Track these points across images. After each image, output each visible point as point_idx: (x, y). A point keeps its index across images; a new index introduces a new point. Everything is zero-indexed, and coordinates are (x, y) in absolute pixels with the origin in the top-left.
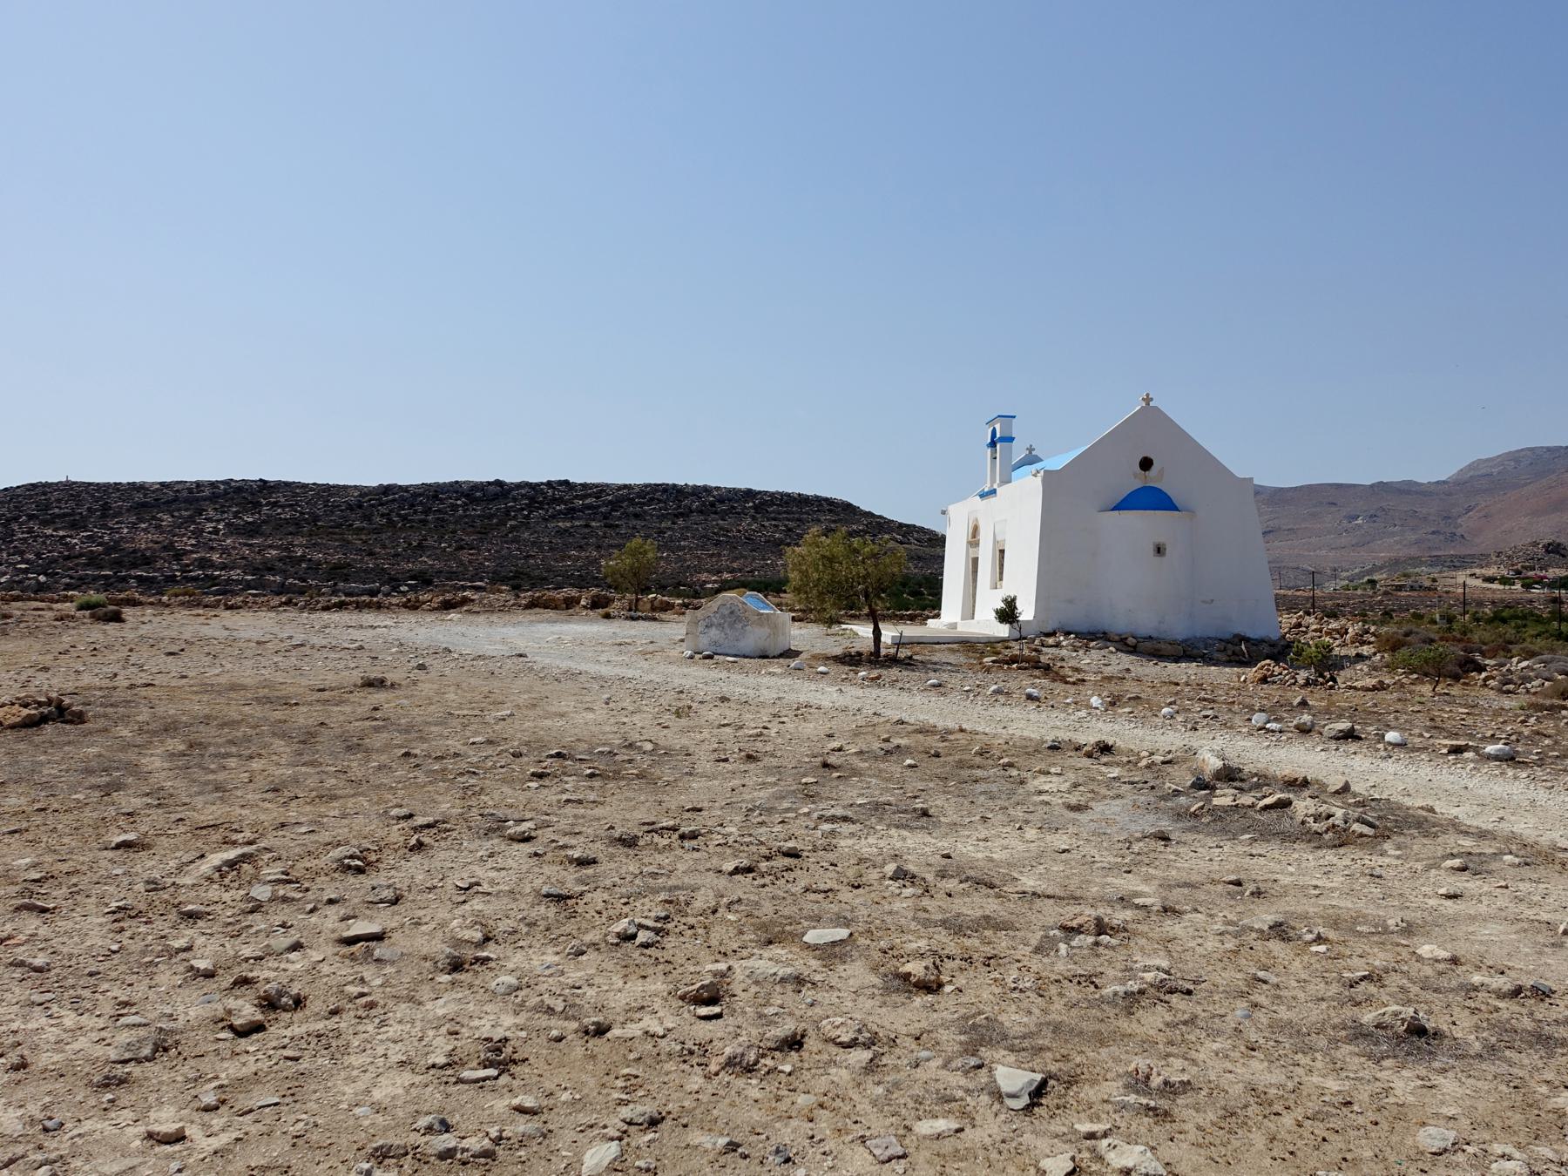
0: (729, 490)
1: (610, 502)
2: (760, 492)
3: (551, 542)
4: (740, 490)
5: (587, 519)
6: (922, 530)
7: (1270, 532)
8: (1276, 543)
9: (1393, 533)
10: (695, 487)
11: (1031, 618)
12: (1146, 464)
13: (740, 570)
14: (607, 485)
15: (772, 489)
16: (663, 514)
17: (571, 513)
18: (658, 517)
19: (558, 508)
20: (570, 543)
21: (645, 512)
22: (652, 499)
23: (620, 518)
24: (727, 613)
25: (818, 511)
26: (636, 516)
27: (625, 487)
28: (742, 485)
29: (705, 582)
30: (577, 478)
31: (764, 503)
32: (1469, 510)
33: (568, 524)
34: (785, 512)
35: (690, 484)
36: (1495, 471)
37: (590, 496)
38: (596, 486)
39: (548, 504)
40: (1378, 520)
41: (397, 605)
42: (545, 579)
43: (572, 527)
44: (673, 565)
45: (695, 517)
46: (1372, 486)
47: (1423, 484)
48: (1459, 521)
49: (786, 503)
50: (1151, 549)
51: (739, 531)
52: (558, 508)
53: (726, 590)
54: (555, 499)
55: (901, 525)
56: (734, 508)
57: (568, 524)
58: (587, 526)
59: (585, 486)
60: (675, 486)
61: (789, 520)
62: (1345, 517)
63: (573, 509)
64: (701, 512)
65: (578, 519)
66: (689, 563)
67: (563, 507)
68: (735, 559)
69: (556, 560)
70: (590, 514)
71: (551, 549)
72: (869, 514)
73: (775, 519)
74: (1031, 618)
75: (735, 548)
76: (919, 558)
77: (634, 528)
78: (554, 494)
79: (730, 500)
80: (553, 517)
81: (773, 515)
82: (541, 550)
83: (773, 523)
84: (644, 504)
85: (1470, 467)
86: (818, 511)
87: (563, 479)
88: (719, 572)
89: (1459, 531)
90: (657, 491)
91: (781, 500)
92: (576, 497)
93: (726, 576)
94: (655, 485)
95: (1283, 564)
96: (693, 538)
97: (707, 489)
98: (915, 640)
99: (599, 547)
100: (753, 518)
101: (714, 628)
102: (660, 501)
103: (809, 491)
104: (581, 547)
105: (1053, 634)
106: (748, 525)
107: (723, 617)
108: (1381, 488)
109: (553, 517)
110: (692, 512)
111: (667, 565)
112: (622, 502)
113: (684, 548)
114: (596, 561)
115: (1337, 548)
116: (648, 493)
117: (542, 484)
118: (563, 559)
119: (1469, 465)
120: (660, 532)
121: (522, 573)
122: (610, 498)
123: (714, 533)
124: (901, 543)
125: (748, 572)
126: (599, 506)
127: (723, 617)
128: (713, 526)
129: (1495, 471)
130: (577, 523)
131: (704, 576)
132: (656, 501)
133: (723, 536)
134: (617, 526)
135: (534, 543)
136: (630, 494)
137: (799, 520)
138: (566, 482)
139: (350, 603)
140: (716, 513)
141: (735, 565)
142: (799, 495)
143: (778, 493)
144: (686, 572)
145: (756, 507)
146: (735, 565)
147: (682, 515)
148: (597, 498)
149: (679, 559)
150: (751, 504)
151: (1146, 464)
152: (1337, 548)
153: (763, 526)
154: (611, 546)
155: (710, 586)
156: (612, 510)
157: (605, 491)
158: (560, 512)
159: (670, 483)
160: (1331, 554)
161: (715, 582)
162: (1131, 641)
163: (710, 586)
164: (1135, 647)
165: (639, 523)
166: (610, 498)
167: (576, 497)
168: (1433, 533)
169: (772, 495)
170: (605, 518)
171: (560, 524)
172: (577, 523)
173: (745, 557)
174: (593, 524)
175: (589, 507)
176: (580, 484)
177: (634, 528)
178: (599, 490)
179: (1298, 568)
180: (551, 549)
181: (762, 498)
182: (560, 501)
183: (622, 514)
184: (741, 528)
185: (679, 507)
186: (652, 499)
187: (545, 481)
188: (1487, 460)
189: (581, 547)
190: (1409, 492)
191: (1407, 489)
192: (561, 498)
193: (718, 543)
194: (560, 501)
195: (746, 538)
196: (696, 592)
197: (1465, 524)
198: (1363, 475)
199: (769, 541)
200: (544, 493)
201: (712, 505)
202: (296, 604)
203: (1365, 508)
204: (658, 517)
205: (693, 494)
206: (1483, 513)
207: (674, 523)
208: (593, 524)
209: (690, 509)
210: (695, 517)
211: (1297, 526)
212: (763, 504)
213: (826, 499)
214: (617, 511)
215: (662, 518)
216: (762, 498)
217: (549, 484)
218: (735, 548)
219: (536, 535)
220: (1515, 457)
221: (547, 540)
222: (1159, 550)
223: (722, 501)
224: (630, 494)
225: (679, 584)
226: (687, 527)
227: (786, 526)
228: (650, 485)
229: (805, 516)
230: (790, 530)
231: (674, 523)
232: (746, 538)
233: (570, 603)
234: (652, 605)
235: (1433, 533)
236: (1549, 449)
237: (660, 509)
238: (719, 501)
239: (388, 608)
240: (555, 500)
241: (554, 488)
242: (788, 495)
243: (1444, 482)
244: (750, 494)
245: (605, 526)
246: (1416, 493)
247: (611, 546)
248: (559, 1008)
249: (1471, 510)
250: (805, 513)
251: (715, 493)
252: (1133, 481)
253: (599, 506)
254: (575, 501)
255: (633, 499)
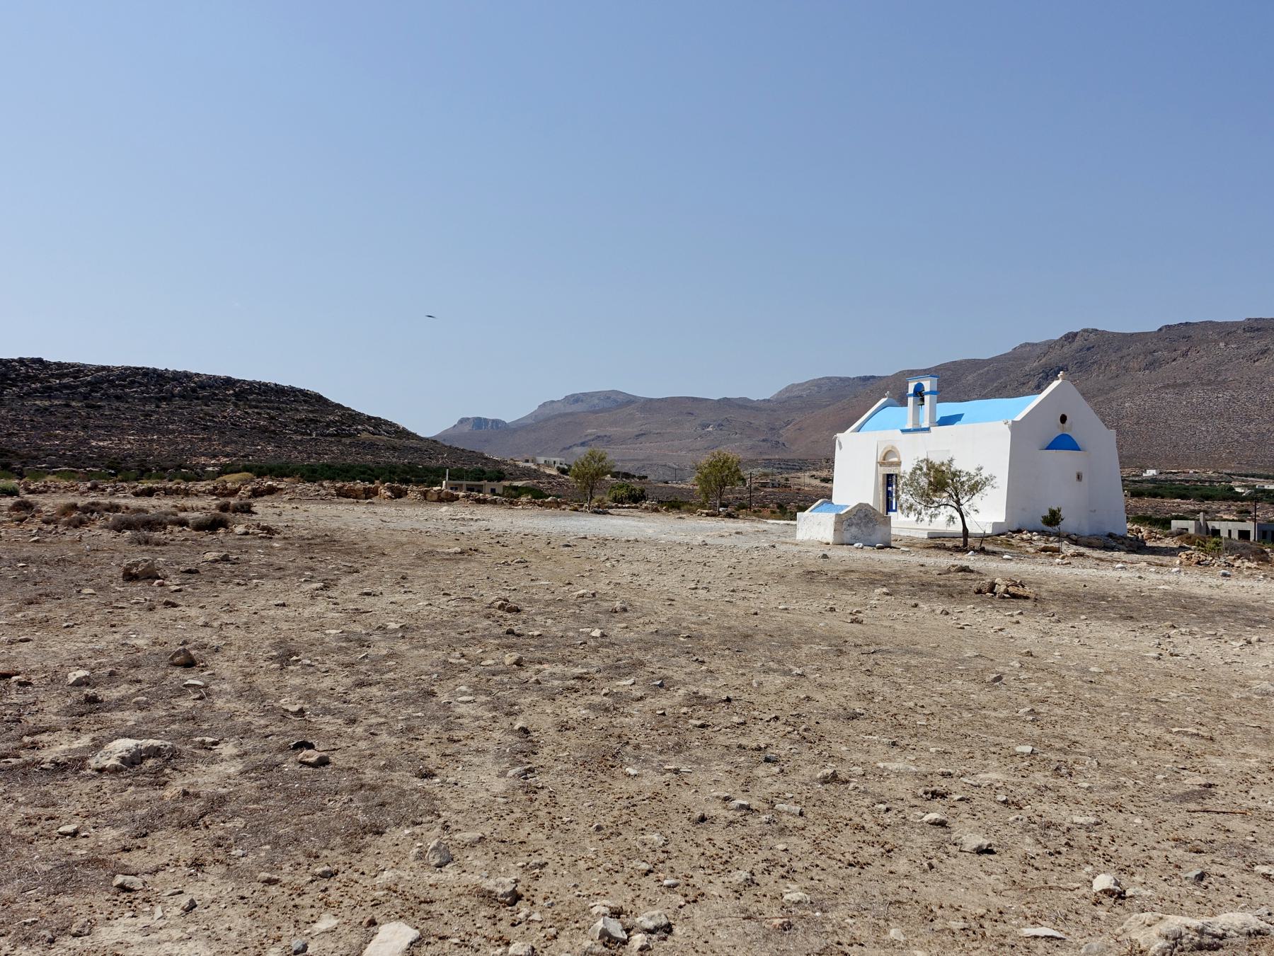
0: (209, 377)
1: (89, 382)
2: (239, 381)
3: (32, 421)
4: (219, 377)
5: (66, 399)
6: (392, 425)
7: (643, 434)
8: (648, 444)
9: (735, 439)
10: (175, 373)
11: (1003, 521)
12: (1063, 419)
13: (235, 455)
14: (84, 366)
15: (249, 379)
16: (145, 397)
17: (48, 392)
18: (140, 400)
19: (33, 386)
20: (53, 422)
21: (126, 394)
22: (133, 382)
23: (101, 399)
24: (862, 515)
25: (294, 401)
26: (118, 398)
27: (104, 368)
28: (222, 372)
29: (205, 466)
30: (51, 357)
31: (243, 391)
32: (788, 423)
33: (47, 403)
34: (264, 401)
35: (171, 369)
36: (804, 394)
37: (67, 375)
38: (73, 366)
39: (22, 381)
40: (724, 428)
41: (204, 492)
42: (36, 458)
43: (51, 406)
44: (167, 447)
45: (177, 402)
46: (719, 401)
47: (754, 401)
48: (781, 432)
49: (264, 392)
50: (1076, 476)
51: (225, 417)
52: (33, 386)
53: (227, 474)
54: (30, 377)
55: (370, 418)
56: (216, 395)
57: (47, 403)
58: (68, 406)
59: (60, 365)
60: (155, 370)
61: (269, 409)
62: (700, 425)
63: (50, 388)
64: (183, 397)
65: (56, 398)
66: (182, 446)
67: (39, 385)
68: (226, 444)
69: (41, 439)
70: (68, 394)
71: (33, 427)
72: (339, 406)
73: (256, 407)
74: (1003, 521)
75: (223, 433)
76: (394, 448)
77: (117, 409)
78: (27, 372)
79: (211, 387)
80: (28, 394)
81: (254, 403)
82: (21, 425)
83: (256, 410)
84: (124, 386)
85: (787, 389)
86: (294, 401)
87: (36, 356)
88: (214, 456)
89: (781, 440)
90: (138, 374)
91: (260, 389)
92: (52, 376)
93: (224, 460)
94: (134, 368)
95: (654, 462)
96: (181, 421)
97: (187, 376)
98: (936, 536)
99: (85, 427)
100: (236, 405)
101: (854, 527)
102: (141, 384)
103: (285, 382)
104: (65, 426)
105: (1019, 531)
106: (232, 411)
107: (860, 518)
108: (726, 402)
109: (28, 394)
110: (173, 396)
111: (160, 447)
112: (102, 383)
113: (173, 432)
114: (84, 442)
115: (693, 450)
116: (129, 376)
117: (14, 360)
118: (49, 437)
119: (786, 388)
120: (147, 415)
121: (9, 451)
122: (89, 379)
123: (200, 418)
124: (374, 434)
125: (242, 456)
126: (78, 387)
127: (860, 518)
128: (198, 411)
129: (804, 394)
130: (56, 402)
131: (202, 460)
132: (137, 385)
133: (210, 421)
134: (100, 407)
135: (13, 421)
136: (109, 376)
137: (278, 408)
138: (40, 361)
139: (159, 489)
140: (198, 398)
141: (228, 449)
142: (276, 385)
143: (255, 382)
144: (181, 455)
145: (236, 395)
146: (228, 449)
147: (164, 399)
148: (75, 378)
149: (171, 442)
150: (231, 392)
151: (1063, 419)
152: (693, 450)
153: (246, 413)
154: (98, 427)
155: (211, 469)
156: (92, 391)
157: (82, 371)
158: (36, 390)
159: (151, 367)
160: (690, 455)
161: (214, 465)
162: (1074, 537)
163: (211, 469)
164: (1076, 541)
165: (123, 406)
166: (89, 379)
167: (52, 376)
168: (764, 440)
169: (250, 383)
170: (86, 398)
171: (37, 402)
172: (56, 402)
173: (236, 442)
174: (74, 404)
175: (66, 386)
176: (55, 363)
177: (117, 409)
178: (77, 371)
179: (665, 465)
180: (33, 427)
181: (241, 387)
182: (35, 379)
183: (103, 395)
184: (226, 414)
185: (161, 391)
186: (133, 382)
187: (16, 358)
188: (798, 385)
189: (65, 426)
190: (745, 407)
191: (742, 405)
192: (35, 376)
193: (205, 428)
194: (35, 379)
195: (232, 424)
196: (197, 474)
197: (786, 434)
198: (714, 391)
199: (255, 428)
200: (16, 370)
201: (194, 390)
202: (104, 490)
203: (714, 418)
204: (140, 400)
205: (174, 379)
206: (797, 427)
207: (158, 407)
208: (74, 404)
209: (172, 393)
210: (177, 402)
211: (664, 431)
212: (243, 392)
213: (301, 391)
214: (97, 392)
215: (145, 401)
216: (241, 387)
217: (21, 361)
218: (223, 433)
219: (14, 413)
220: (818, 384)
221: (27, 418)
222: (1079, 477)
223: (203, 387)
224: (109, 376)
225: (180, 467)
226: (172, 411)
227: (268, 414)
228: (129, 368)
229: (284, 406)
230: (273, 418)
231: (158, 407)
232: (232, 424)
233: (369, 494)
234: (439, 496)
235: (764, 440)
236: (841, 379)
237: (143, 392)
238: (199, 387)
239: (196, 495)
240: (28, 378)
241: (26, 365)
242: (266, 385)
243: (769, 400)
244: (229, 382)
245: (87, 407)
246: (752, 408)
247: (98, 427)
248: (33, 903)
249: (789, 424)
250: (283, 403)
251: (196, 379)
252: (1056, 430)
253: (78, 387)
254: (51, 380)
255: (113, 381)
